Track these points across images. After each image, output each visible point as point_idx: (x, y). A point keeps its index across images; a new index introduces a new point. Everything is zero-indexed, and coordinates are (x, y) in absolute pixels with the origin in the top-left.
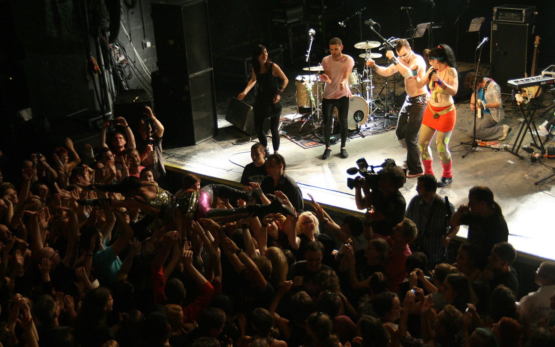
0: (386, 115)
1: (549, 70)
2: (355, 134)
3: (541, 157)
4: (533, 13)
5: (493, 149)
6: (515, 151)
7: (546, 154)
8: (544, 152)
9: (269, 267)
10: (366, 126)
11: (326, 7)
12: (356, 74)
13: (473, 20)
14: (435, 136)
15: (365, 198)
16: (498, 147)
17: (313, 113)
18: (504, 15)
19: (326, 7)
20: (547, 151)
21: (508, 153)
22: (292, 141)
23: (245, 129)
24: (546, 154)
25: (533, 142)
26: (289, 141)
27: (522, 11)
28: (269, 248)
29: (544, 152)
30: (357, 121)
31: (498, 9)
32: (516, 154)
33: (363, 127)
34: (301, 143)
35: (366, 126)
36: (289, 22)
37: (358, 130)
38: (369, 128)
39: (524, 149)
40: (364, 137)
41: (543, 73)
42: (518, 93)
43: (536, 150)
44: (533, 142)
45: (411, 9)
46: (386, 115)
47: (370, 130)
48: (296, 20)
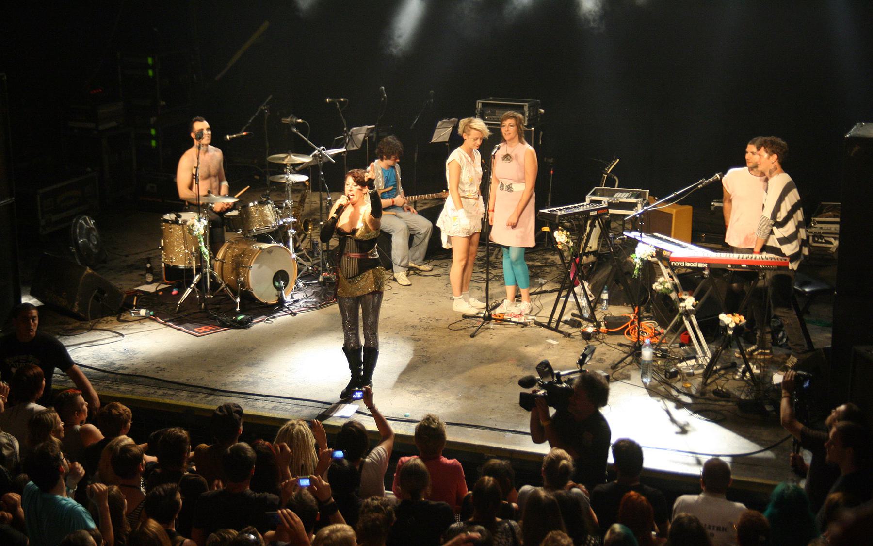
0: (321, 279)
1: (594, 194)
2: (277, 312)
3: (598, 332)
4: (537, 110)
5: (517, 323)
6: (554, 325)
7: (603, 328)
8: (598, 325)
9: (416, 466)
10: (292, 298)
11: (163, 103)
12: (273, 208)
13: (440, 123)
14: (142, 394)
15: (158, 460)
16: (522, 321)
17: (196, 278)
18: (493, 113)
19: (163, 103)
20: (603, 324)
21: (543, 328)
22: (169, 326)
23: (76, 309)
24: (603, 328)
25: (576, 312)
26: (163, 326)
27: (522, 107)
28: (393, 437)
29: (598, 325)
30: (279, 289)
31: (483, 104)
32: (556, 330)
33: (287, 299)
34: (187, 328)
35: (292, 298)
36: (101, 128)
37: (281, 303)
38: (297, 301)
39: (566, 322)
40: (295, 314)
41: (588, 198)
42: (558, 230)
43: (584, 323)
44: (576, 312)
45: (345, 102)
46: (321, 279)
47: (301, 303)
48: (113, 124)
